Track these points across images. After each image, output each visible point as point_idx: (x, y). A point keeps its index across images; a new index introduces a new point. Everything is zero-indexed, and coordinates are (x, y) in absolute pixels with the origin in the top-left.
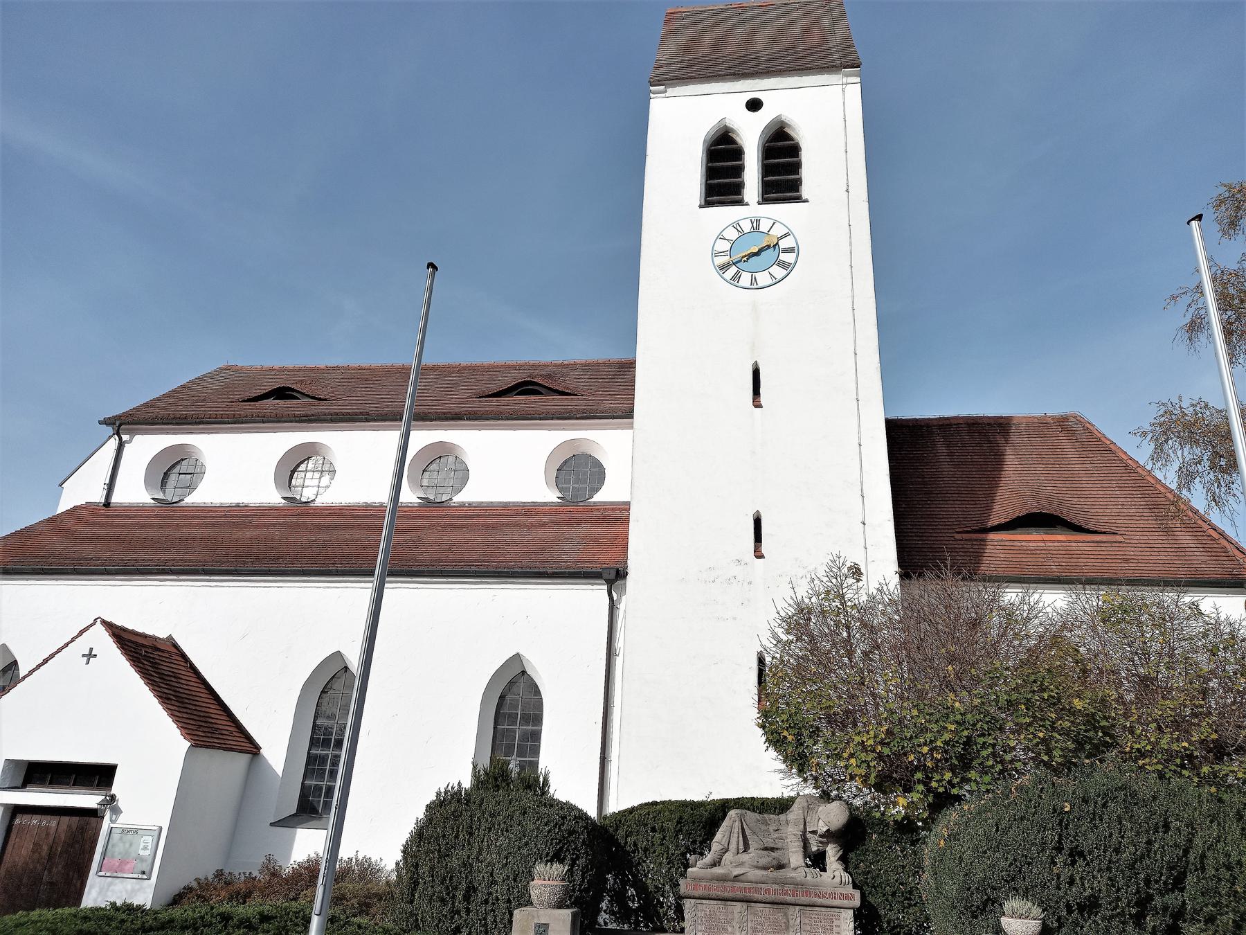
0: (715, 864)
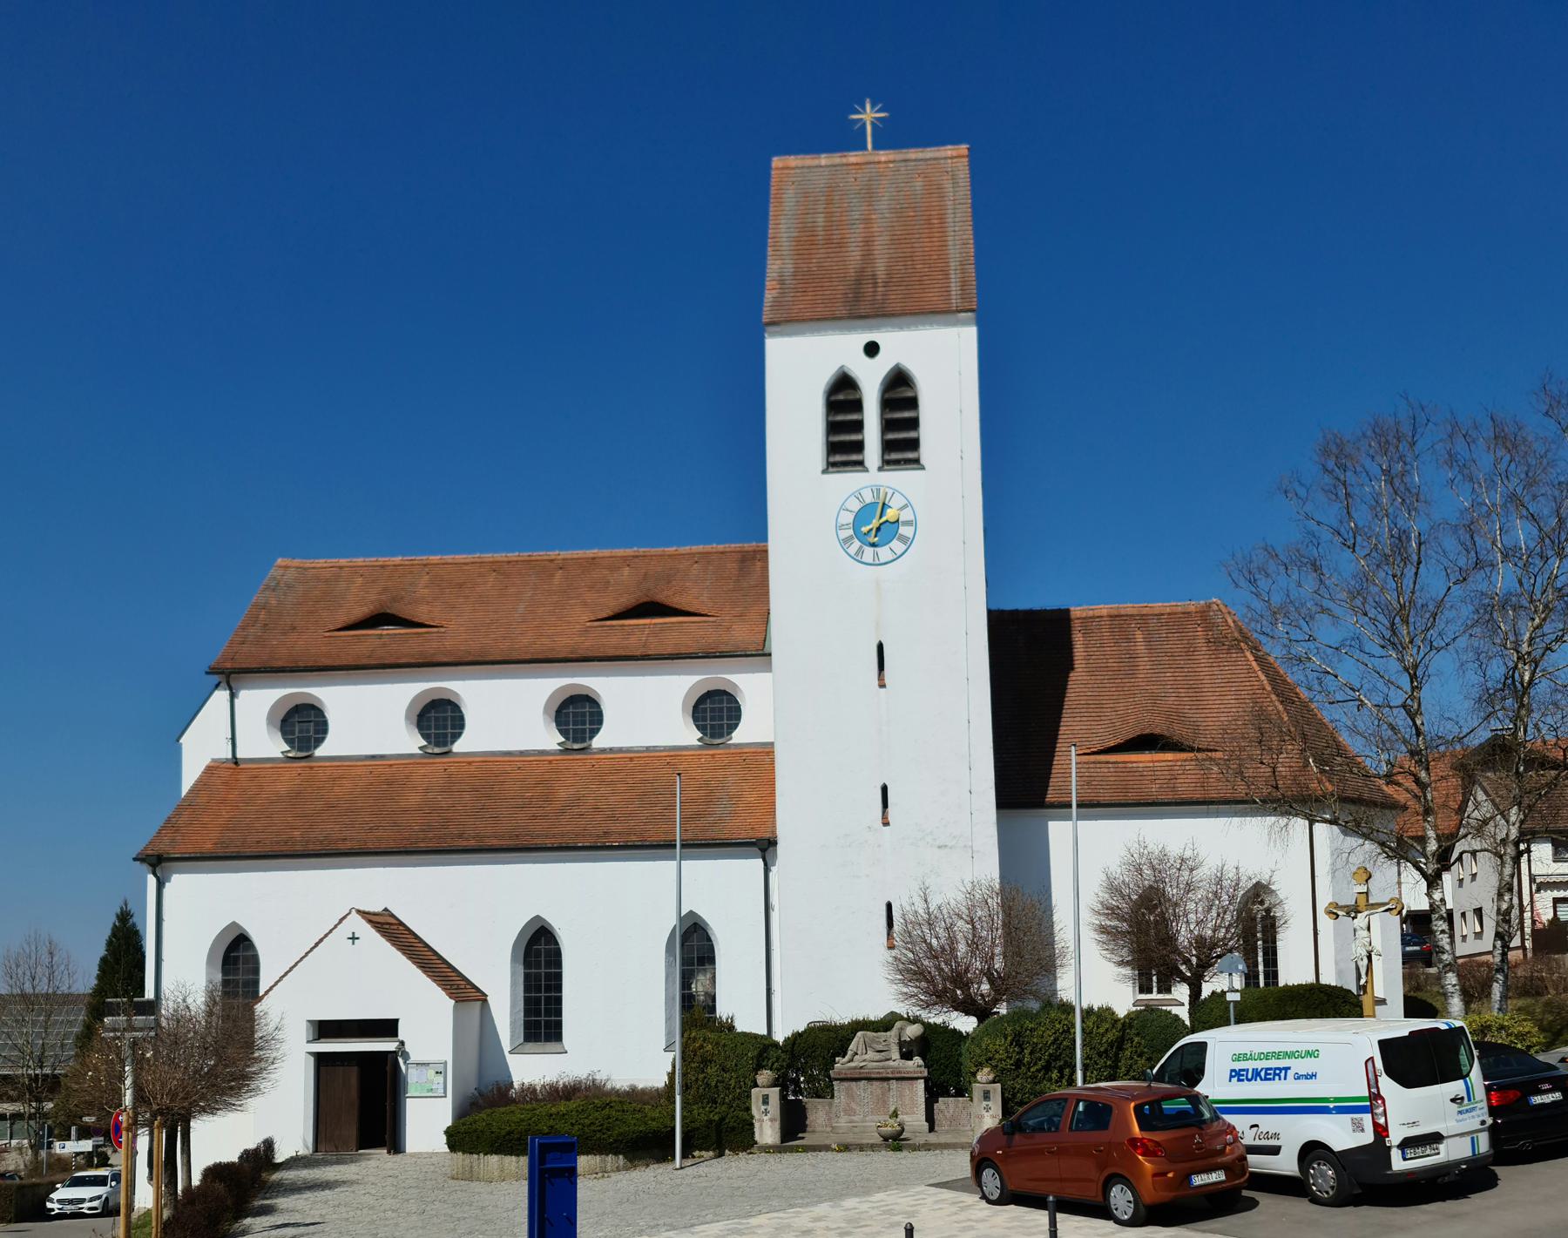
0: (851, 1060)
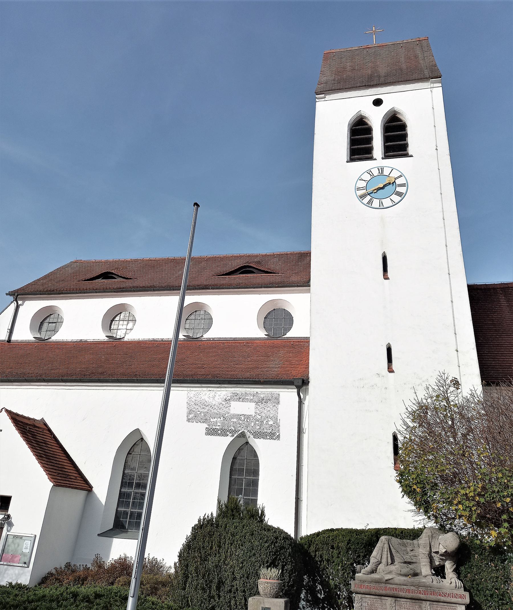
0: (373, 571)
